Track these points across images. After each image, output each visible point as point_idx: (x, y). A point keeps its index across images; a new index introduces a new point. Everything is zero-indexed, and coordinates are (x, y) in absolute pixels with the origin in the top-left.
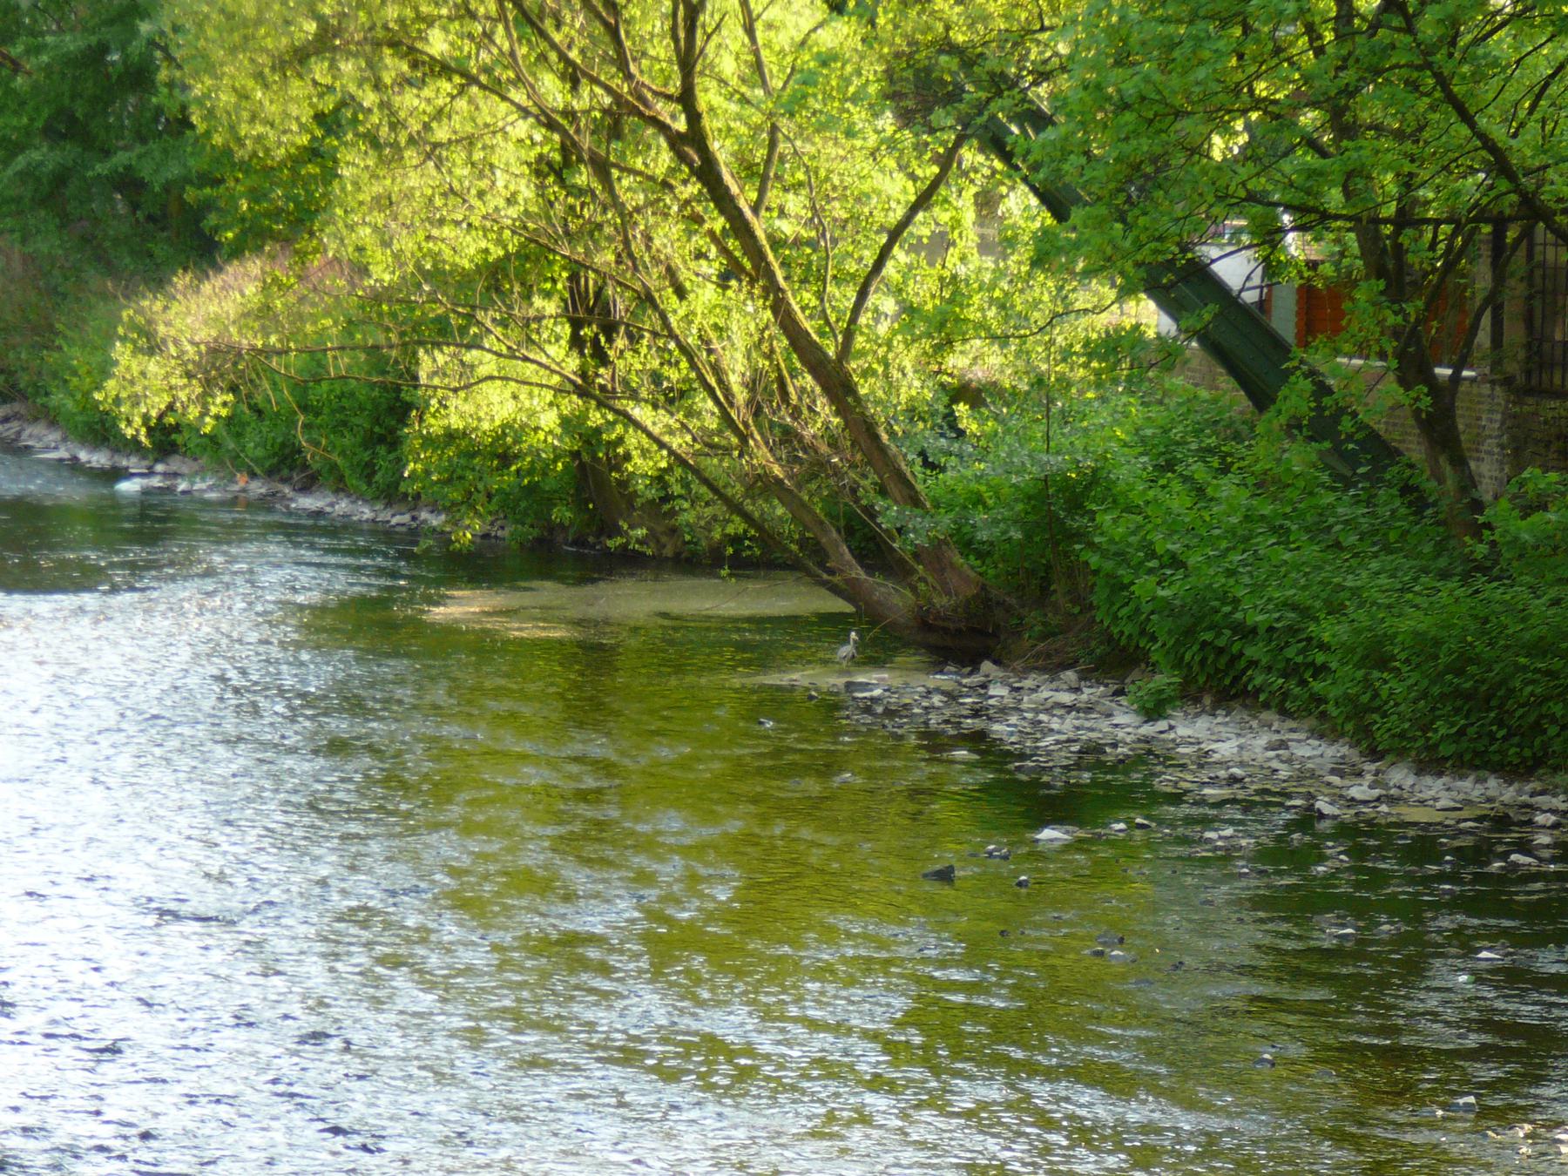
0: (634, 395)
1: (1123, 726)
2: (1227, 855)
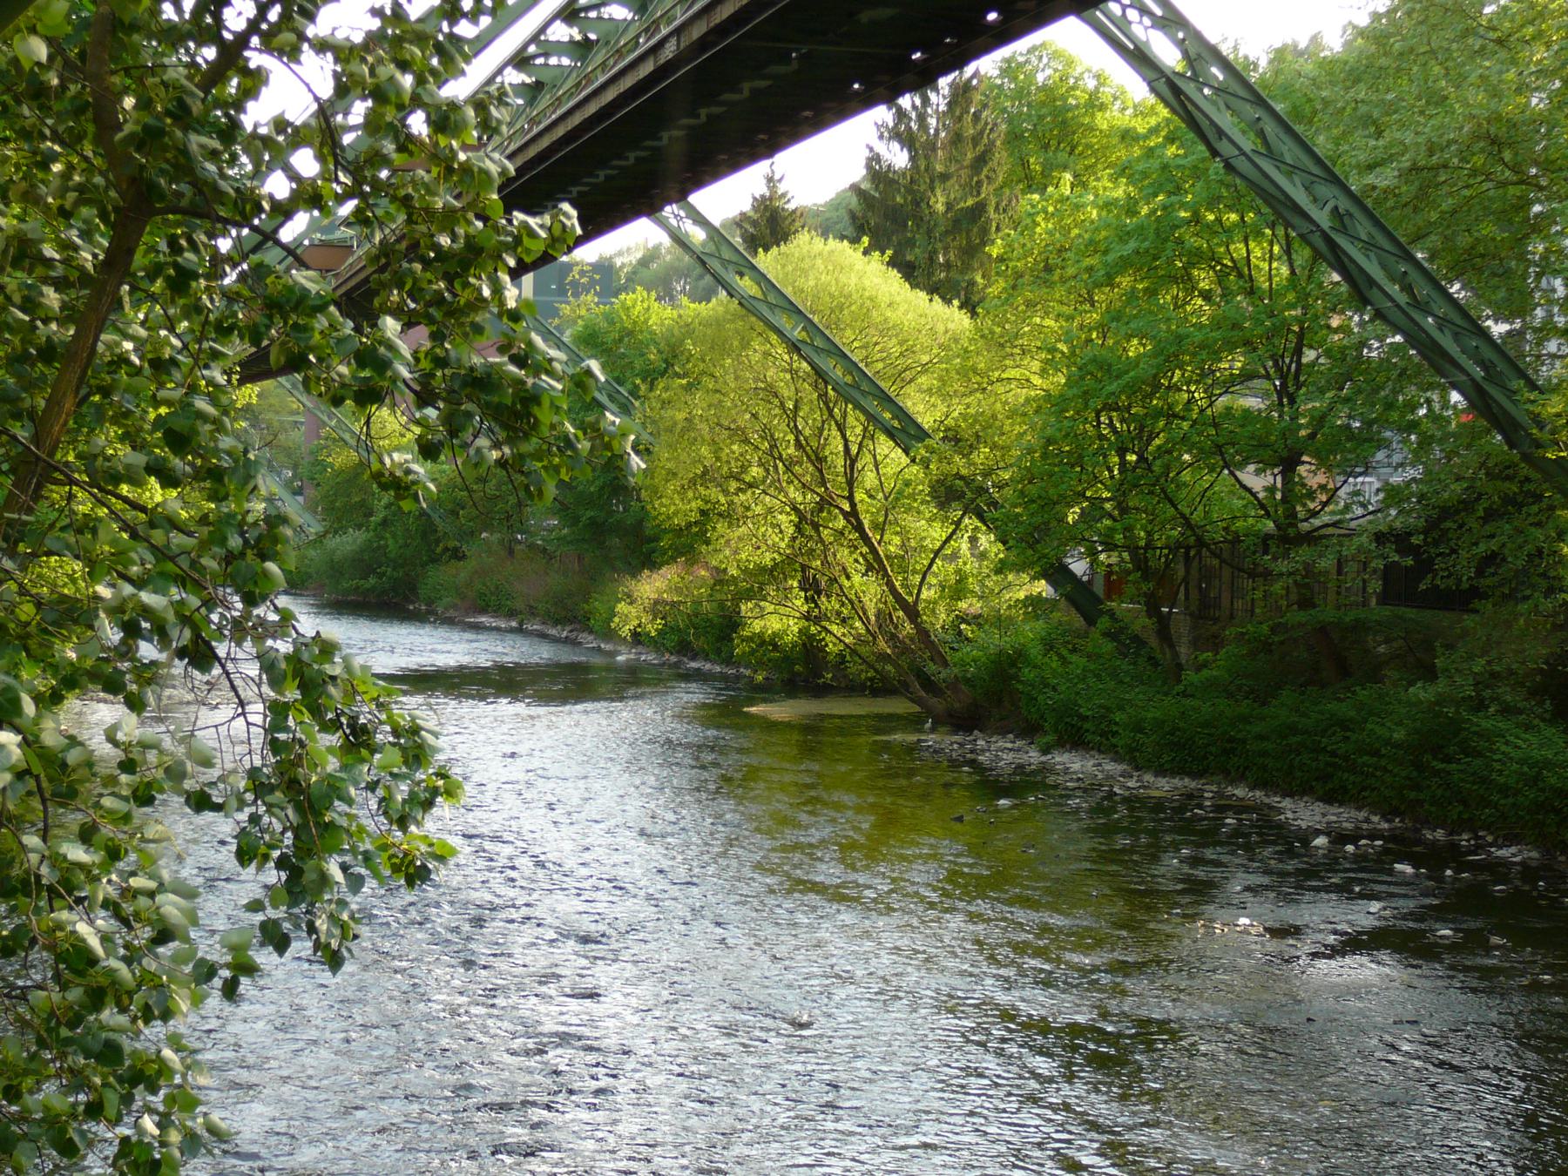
0: (828, 619)
1: (1033, 757)
2: (1077, 810)
